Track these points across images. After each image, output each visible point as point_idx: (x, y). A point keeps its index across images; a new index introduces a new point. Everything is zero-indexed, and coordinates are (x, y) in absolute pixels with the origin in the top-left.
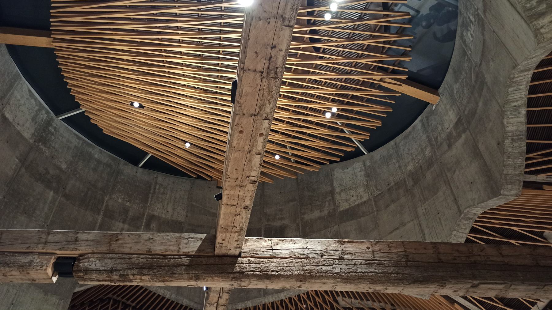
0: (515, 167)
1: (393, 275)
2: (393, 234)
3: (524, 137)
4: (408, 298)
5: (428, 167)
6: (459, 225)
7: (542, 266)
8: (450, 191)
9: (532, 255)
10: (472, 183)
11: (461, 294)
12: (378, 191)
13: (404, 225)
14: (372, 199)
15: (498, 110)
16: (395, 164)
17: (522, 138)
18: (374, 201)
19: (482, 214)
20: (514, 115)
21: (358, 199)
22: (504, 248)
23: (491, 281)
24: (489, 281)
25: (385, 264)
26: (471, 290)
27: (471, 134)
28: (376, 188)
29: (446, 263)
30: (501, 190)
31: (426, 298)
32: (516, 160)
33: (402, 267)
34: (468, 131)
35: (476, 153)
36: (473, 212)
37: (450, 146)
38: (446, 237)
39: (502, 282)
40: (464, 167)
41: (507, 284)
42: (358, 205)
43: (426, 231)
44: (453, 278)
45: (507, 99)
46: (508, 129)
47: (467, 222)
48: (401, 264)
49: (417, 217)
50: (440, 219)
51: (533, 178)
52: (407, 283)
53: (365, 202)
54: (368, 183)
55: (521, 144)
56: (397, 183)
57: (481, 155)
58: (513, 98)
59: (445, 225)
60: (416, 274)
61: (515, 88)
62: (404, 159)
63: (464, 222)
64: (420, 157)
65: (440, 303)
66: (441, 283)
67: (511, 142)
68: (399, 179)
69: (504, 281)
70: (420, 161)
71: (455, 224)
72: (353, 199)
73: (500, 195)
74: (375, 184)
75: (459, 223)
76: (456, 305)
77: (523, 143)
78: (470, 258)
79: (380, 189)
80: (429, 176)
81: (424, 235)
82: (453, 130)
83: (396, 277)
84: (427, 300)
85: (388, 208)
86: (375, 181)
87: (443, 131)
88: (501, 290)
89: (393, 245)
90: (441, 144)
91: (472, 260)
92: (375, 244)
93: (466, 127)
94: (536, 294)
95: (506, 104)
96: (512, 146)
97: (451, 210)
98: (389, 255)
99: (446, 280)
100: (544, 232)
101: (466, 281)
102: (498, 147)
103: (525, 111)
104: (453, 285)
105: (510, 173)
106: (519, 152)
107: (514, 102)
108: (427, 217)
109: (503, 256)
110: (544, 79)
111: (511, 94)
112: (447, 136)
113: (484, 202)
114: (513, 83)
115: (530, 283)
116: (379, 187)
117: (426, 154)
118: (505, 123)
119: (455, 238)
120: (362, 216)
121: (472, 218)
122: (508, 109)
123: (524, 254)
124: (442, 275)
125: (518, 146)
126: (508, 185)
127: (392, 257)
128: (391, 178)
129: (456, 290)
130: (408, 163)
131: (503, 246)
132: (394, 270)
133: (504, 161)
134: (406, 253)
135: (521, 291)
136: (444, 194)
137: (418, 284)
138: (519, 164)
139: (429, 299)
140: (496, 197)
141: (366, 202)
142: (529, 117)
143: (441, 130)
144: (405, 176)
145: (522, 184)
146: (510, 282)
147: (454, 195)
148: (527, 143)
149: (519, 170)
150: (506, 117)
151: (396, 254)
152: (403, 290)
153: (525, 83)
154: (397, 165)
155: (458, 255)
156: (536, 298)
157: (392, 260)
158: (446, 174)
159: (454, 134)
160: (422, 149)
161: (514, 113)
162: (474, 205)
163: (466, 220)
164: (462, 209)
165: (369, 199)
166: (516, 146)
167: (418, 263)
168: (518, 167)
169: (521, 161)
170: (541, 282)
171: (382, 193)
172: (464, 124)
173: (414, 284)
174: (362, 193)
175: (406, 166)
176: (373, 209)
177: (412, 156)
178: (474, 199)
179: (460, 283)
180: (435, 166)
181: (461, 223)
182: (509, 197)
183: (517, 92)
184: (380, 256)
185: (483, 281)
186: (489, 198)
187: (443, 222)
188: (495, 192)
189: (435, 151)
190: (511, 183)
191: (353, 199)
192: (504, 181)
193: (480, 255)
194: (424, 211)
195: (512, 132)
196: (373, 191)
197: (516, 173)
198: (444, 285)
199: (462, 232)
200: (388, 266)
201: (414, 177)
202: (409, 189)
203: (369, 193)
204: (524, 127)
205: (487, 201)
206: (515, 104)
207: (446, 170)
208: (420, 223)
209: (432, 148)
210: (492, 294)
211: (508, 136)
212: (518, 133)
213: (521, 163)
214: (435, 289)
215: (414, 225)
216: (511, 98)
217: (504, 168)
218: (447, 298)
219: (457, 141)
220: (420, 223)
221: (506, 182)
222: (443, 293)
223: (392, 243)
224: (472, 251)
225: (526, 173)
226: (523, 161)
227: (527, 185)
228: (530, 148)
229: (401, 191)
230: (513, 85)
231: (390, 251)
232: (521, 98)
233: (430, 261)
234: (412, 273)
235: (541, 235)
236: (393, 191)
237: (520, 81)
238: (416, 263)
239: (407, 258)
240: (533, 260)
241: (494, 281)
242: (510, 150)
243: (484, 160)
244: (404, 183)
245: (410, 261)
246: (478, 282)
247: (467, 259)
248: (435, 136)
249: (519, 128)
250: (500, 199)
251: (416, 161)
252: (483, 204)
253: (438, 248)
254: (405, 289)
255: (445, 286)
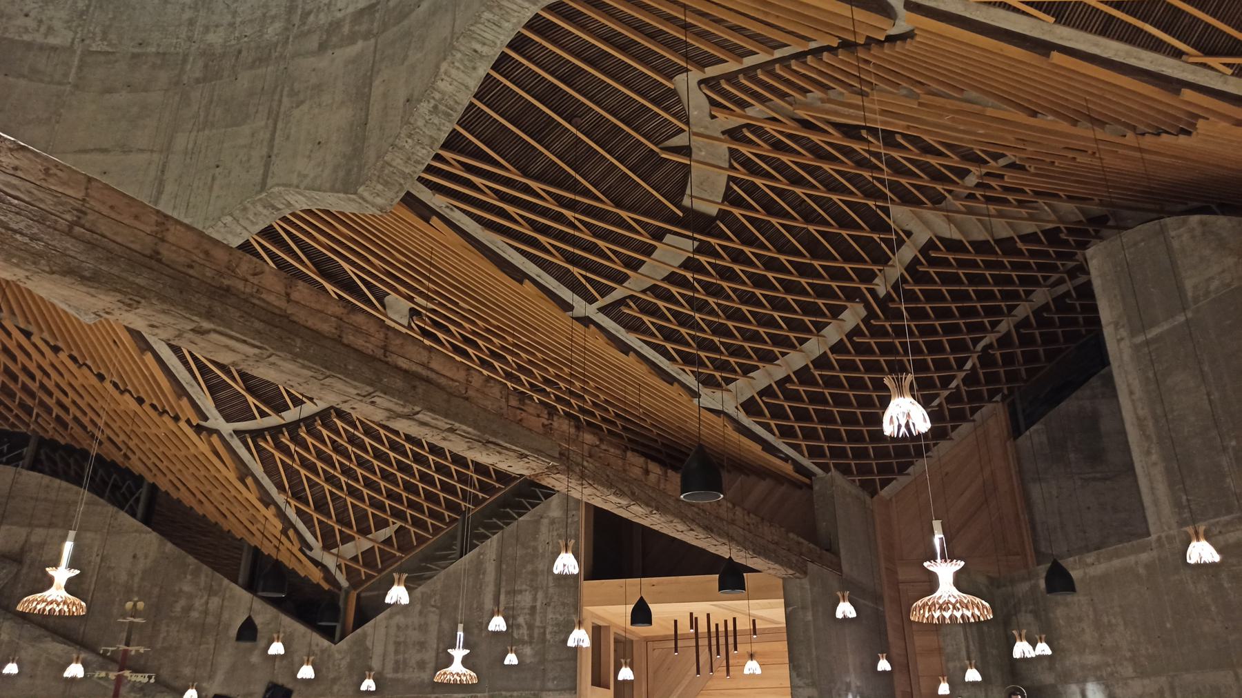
0: (409, 159)
1: (18, 236)
2: (88, 156)
3: (456, 116)
4: (46, 306)
5: (254, 62)
6: (245, 209)
7: (344, 345)
8: (268, 135)
9: (341, 319)
10: (319, 143)
11: (165, 336)
12: (105, 43)
13: (124, 152)
14: (79, 52)
15: (445, 39)
16: (183, 10)
17: (451, 115)
18: (81, 60)
19: (303, 211)
20: (465, 66)
21: (38, 31)
22: (300, 288)
23: (238, 335)
24: (233, 333)
25: (11, 204)
26: (191, 335)
27: (375, 52)
28: (105, 33)
29: (168, 266)
30: (361, 186)
31: (88, 319)
32: (418, 148)
33: (55, 229)
34: (373, 41)
35: (361, 96)
36: (289, 199)
37: (323, 47)
38: (206, 219)
39: (258, 344)
40: (324, 104)
41: (264, 351)
42: (29, 46)
43: (169, 188)
44: (163, 298)
45: (472, 28)
46: (439, 83)
47: (265, 212)
48: (56, 222)
49: (167, 149)
50: (214, 178)
51: (425, 195)
52: (47, 269)
53: (54, 49)
54: (87, 11)
55: (444, 124)
56: (164, 54)
57: (368, 102)
58: (482, 33)
59: (218, 197)
60: (82, 258)
61: (496, 18)
62: (213, 13)
63: (260, 208)
64: (248, 31)
65: (115, 342)
66: (131, 299)
67: (429, 111)
68: (175, 47)
69: (261, 343)
70: (246, 39)
71: (240, 204)
72: (21, 21)
73: (355, 193)
74: (108, 23)
75: (249, 205)
76: (148, 357)
77: (447, 124)
78: (224, 278)
79: (114, 42)
80: (244, 80)
81: (160, 193)
82: (348, 21)
83: (26, 244)
84: (89, 326)
85: (107, 96)
86: (110, 16)
87: (328, 9)
88: (247, 356)
89: (59, 173)
90: (309, 31)
91: (226, 282)
92: (11, 150)
93: (375, 31)
94: (305, 385)
95: (464, 37)
96: (427, 118)
97: (248, 172)
98: (36, 192)
99: (144, 298)
100: (389, 294)
101: (187, 316)
102: (405, 105)
103: (485, 71)
104: (154, 313)
105: (394, 164)
106: (431, 137)
107: (479, 42)
108: (188, 160)
109: (289, 301)
110: (546, 37)
111: (483, 24)
112: (331, 24)
113: (320, 191)
114: (498, 6)
115: (306, 363)
116: (113, 36)
117: (267, 33)
118: (442, 70)
119: (223, 230)
120: (24, 76)
121: (279, 209)
122: (463, 48)
123: (329, 313)
124: (142, 284)
125: (436, 125)
126: (379, 182)
127: (41, 199)
128: (157, 33)
129: (155, 324)
130: (217, 26)
131: (300, 283)
132: (28, 227)
133: (398, 136)
134: (83, 205)
135: (283, 372)
136: (253, 135)
137: (73, 281)
138: (419, 159)
139: (95, 324)
140: (346, 193)
141: (57, 48)
142: (483, 89)
143: (325, 5)
144: (193, 48)
145: (403, 194)
146: (273, 348)
147: (271, 147)
148: (454, 130)
149: (413, 169)
150: (450, 58)
151: (56, 196)
152: (27, 277)
153: (515, 20)
154: (188, 14)
155: (202, 262)
156: (302, 392)
157: (37, 203)
158: (281, 96)
159: (346, 29)
160: (264, 15)
161: (467, 63)
162: (298, 187)
163: (265, 207)
164: (270, 182)
165: (70, 49)
166: (433, 123)
167: (99, 238)
168: (415, 162)
169: (425, 156)
170: (326, 368)
171: (114, 53)
172: (375, 24)
173: (65, 276)
174: (57, 24)
175: (207, 29)
176: (66, 75)
177: (234, 17)
178: (305, 176)
179: (174, 316)
180: (269, 68)
181: (252, 207)
182: (368, 205)
183: (494, 27)
184: (9, 182)
185: (221, 329)
186: (333, 189)
187: (216, 188)
188: (348, 186)
189: (288, 38)
190: (386, 184)
191: (21, 21)
192: (376, 172)
193: (246, 280)
194: (190, 146)
195: (443, 93)
196: (91, 35)
197: (404, 169)
198: (135, 306)
199: (245, 225)
200: (17, 213)
201: (211, 63)
202: (185, 82)
203: (79, 35)
204: (466, 99)
205: (325, 191)
206: (478, 47)
207: (287, 89)
208: (164, 166)
209: (286, 29)
210: (225, 358)
211: (432, 95)
212: (452, 103)
213: (423, 159)
214: (109, 305)
215: (149, 164)
216: (479, 32)
217: (390, 149)
218: (136, 335)
219: (341, 47)
220: (164, 166)
221: (379, 177)
222: (124, 320)
223: (61, 170)
224: (237, 266)
225: (420, 179)
226: (428, 156)
227: (410, 201)
228: (454, 142)
229: (163, 76)
230: (496, 10)
231: (44, 184)
232: (493, 44)
233: (132, 246)
234: (72, 253)
235: (381, 297)
236: (145, 67)
237: (510, 11)
238: (95, 236)
239: (79, 218)
240: (336, 329)
241: (245, 336)
242: (420, 123)
243: (367, 115)
244: (179, 62)
245: (83, 226)
246: (212, 326)
247: (217, 277)
248: (308, 8)
249: (457, 94)
250: (350, 200)
251: (236, 35)
252: (314, 194)
253: (168, 230)
254: (36, 278)
255: (136, 309)
